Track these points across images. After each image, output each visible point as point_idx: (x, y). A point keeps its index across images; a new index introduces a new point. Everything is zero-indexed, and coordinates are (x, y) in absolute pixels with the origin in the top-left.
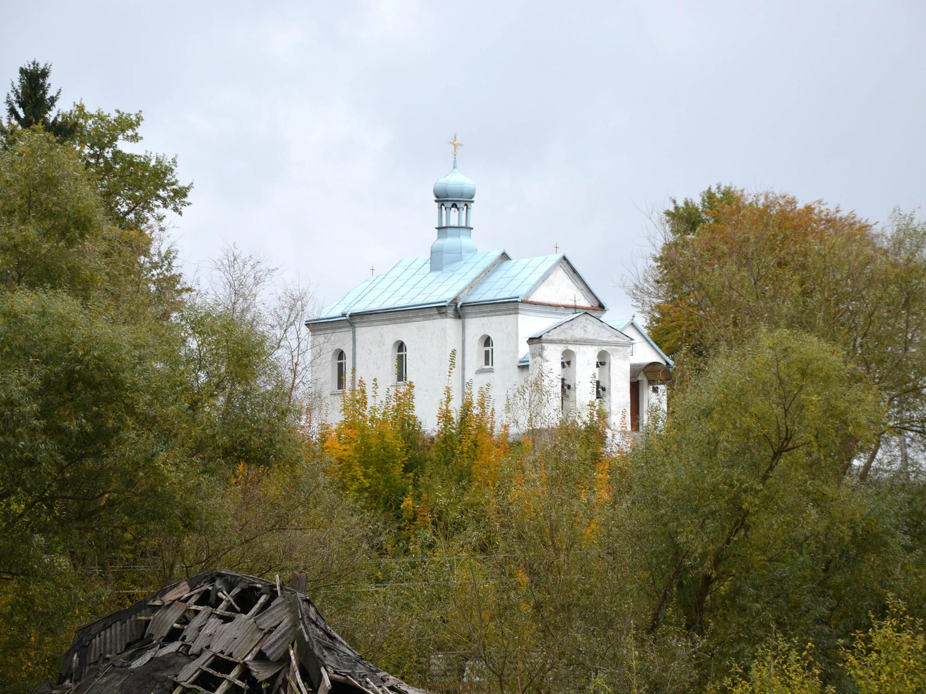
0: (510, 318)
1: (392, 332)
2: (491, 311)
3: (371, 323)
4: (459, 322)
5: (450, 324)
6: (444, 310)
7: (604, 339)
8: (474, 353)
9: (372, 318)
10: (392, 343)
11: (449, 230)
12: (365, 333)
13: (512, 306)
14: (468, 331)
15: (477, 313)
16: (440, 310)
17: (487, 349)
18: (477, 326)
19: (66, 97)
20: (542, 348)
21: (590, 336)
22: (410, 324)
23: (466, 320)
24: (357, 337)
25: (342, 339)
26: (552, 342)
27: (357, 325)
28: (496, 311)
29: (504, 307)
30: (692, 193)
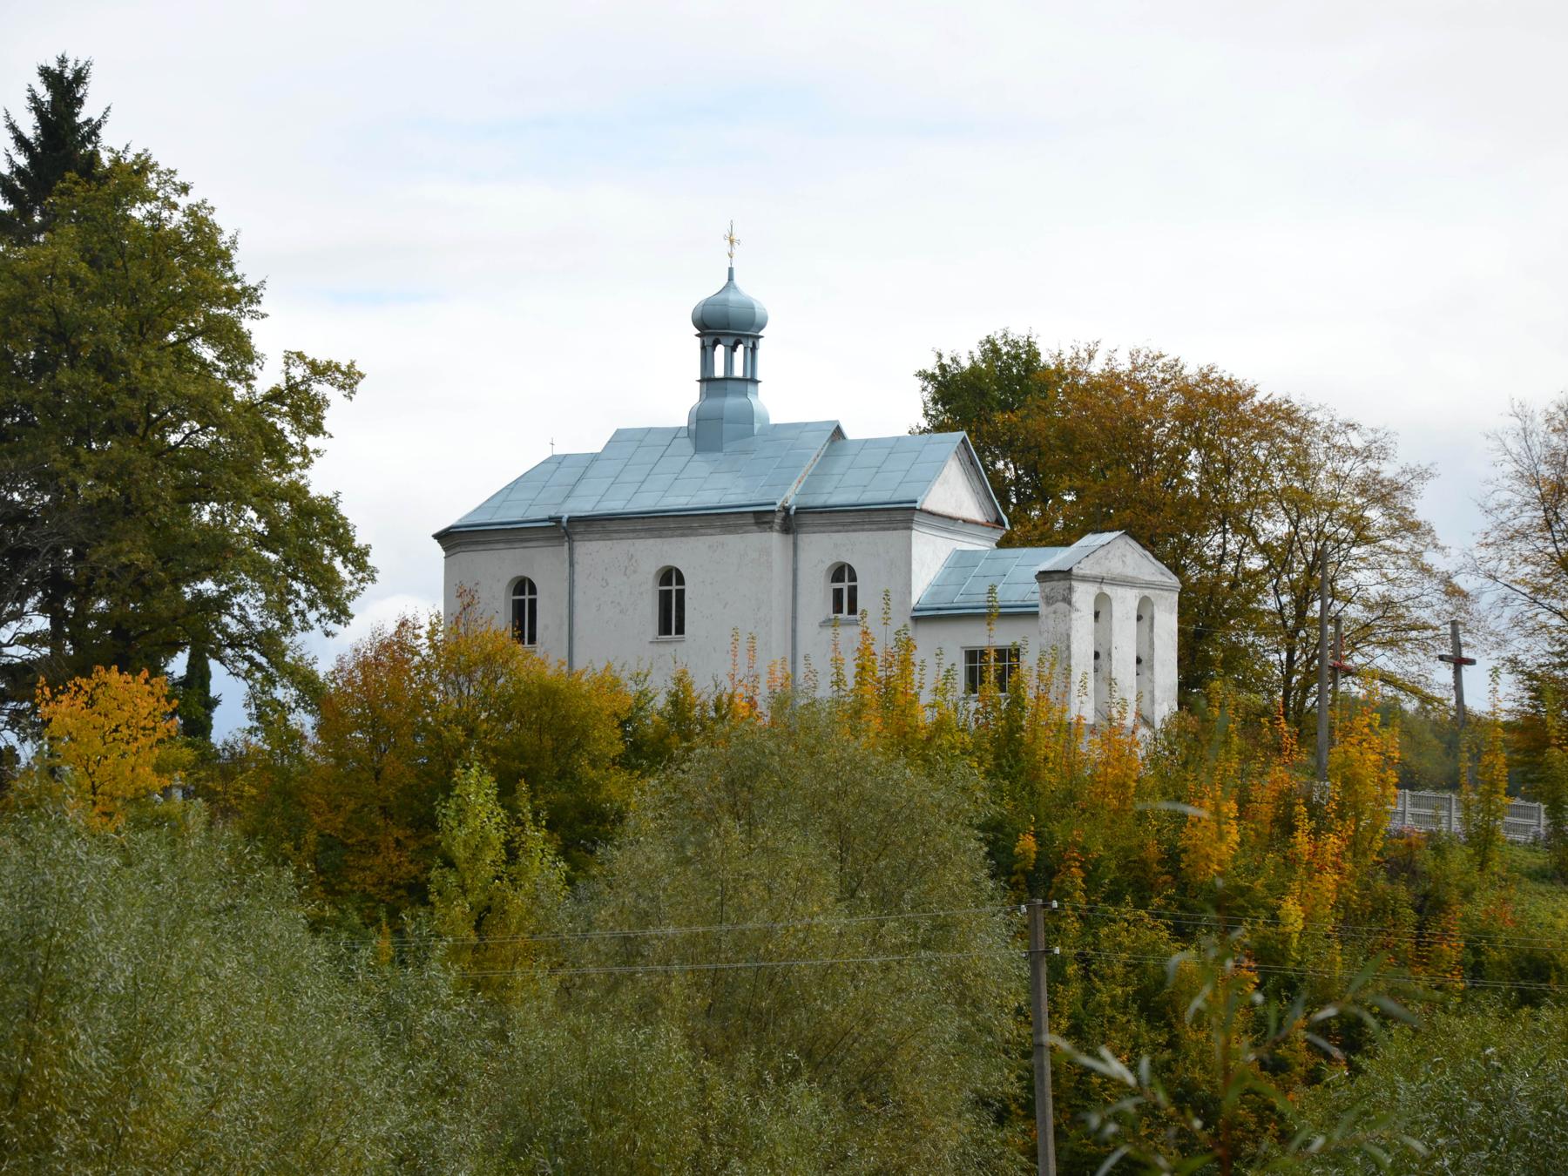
0: (894, 536)
1: (654, 553)
2: (853, 523)
3: (606, 535)
4: (790, 537)
5: (774, 540)
6: (768, 518)
7: (1147, 578)
8: (817, 595)
9: (612, 526)
10: (654, 570)
11: (730, 385)
12: (591, 552)
13: (899, 516)
14: (802, 555)
15: (824, 525)
16: (761, 518)
17: (838, 585)
18: (822, 550)
19: (121, 125)
20: (1070, 589)
21: (1130, 571)
22: (651, 541)
23: (801, 536)
24: (576, 556)
25: (543, 565)
26: (1084, 579)
27: (576, 537)
28: (864, 523)
29: (884, 517)
30: (965, 350)
